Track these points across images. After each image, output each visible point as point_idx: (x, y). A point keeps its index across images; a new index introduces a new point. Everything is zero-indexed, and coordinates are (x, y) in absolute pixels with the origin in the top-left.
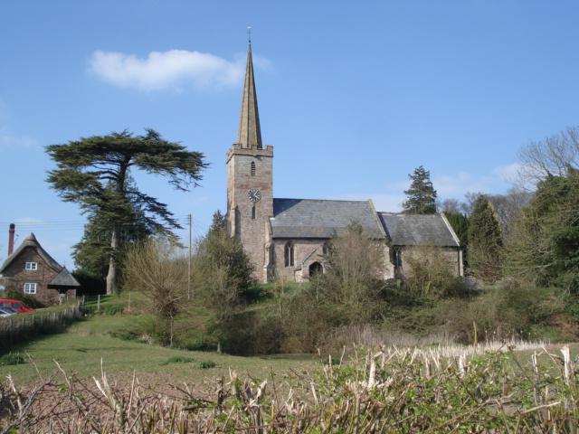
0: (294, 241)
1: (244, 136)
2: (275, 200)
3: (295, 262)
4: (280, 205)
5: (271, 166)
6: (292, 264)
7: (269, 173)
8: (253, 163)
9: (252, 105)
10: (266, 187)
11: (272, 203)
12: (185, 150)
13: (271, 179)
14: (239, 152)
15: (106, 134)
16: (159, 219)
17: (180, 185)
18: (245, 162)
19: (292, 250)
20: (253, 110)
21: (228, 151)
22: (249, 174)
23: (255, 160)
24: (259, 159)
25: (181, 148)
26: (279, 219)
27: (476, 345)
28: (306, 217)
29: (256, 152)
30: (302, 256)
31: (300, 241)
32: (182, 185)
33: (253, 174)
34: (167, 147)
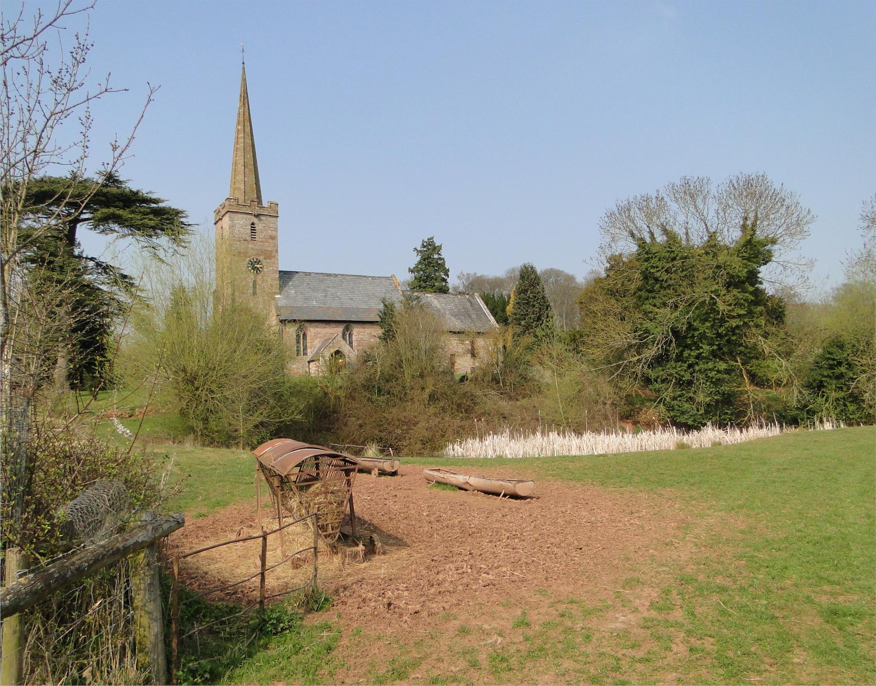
0: (353, 325)
1: (239, 189)
2: (280, 272)
3: (309, 351)
4: (286, 276)
5: (276, 230)
6: (305, 354)
7: (273, 238)
8: (253, 224)
9: (249, 148)
10: (271, 255)
11: (277, 276)
12: (161, 205)
13: (276, 245)
14: (230, 208)
15: (60, 176)
16: (123, 297)
17: (158, 252)
18: (242, 222)
19: (304, 335)
20: (250, 155)
21: (217, 206)
22: (249, 239)
23: (255, 220)
24: (260, 220)
25: (156, 201)
26: (287, 297)
27: (548, 435)
28: (320, 295)
29: (257, 211)
30: (317, 343)
31: (316, 324)
32: (161, 253)
33: (253, 238)
34: (131, 200)
